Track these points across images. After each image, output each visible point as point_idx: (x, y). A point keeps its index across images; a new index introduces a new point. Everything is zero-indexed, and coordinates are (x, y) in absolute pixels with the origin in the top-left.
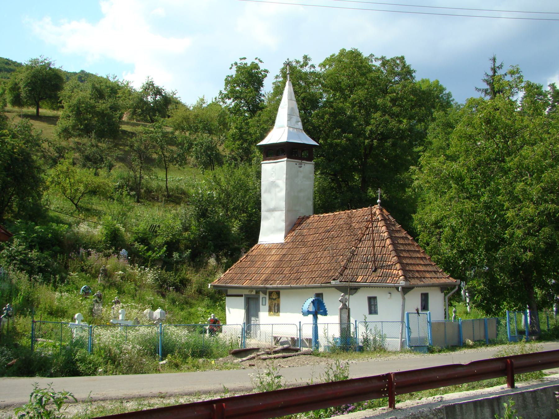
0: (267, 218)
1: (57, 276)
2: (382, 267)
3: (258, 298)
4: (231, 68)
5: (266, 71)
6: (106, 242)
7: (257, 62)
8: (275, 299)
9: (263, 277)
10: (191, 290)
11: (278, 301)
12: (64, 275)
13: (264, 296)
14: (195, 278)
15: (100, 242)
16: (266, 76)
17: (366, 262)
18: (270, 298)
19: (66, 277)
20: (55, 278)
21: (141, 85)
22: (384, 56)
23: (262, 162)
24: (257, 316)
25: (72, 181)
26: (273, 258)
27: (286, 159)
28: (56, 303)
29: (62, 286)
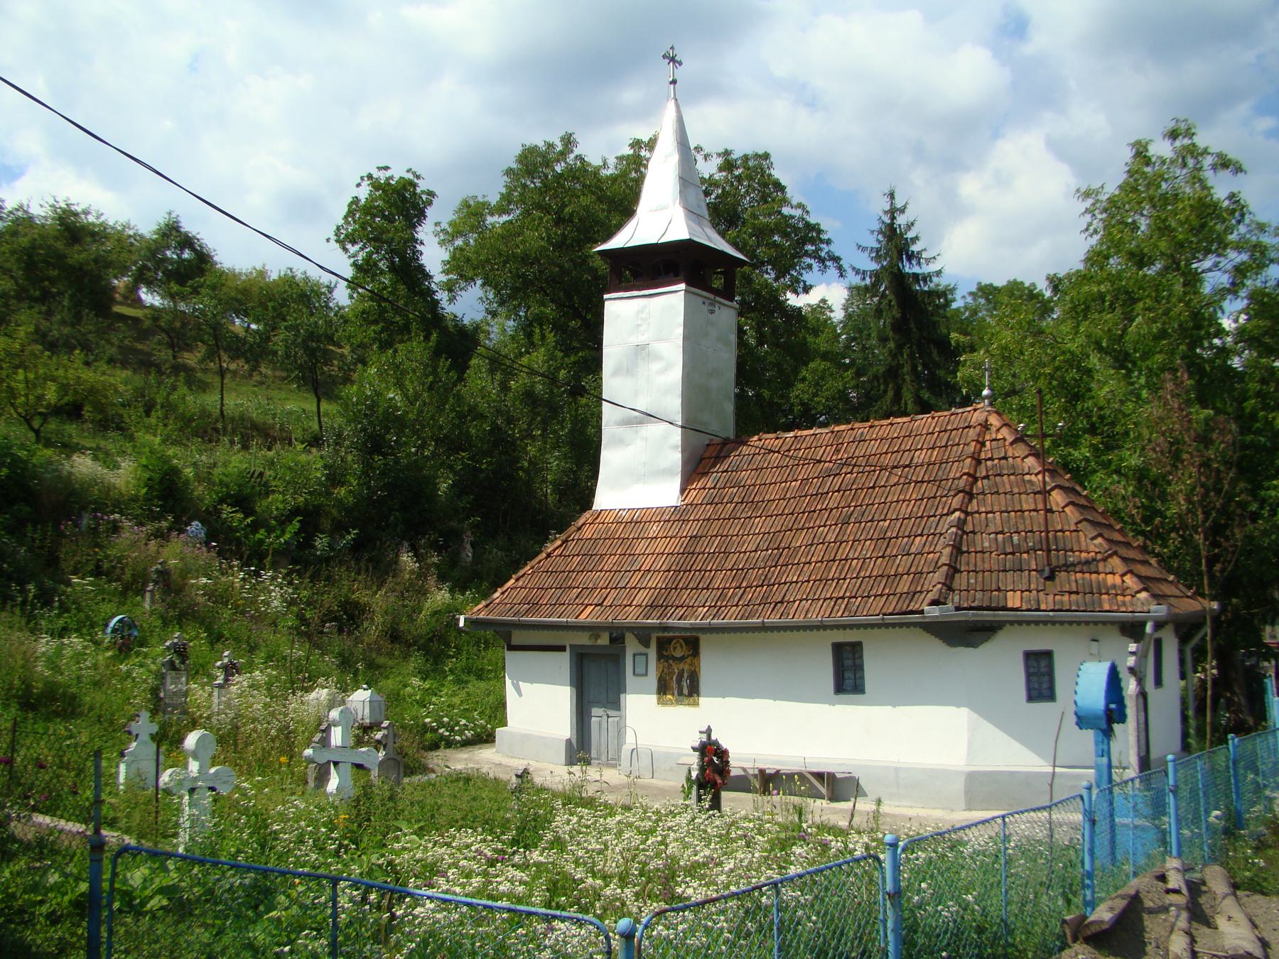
0: (621, 442)
1: (31, 587)
2: (1068, 567)
3: (618, 655)
4: (359, 185)
5: (431, 194)
6: (148, 499)
7: (410, 176)
8: (682, 659)
9: (642, 598)
10: (373, 629)
11: (691, 665)
12: (49, 583)
13: (642, 649)
14: (379, 601)
15: (135, 499)
16: (430, 203)
17: (1013, 553)
18: (660, 656)
19: (54, 591)
20: (23, 591)
21: (155, 227)
22: (729, 149)
23: (606, 296)
24: (614, 703)
25: (31, 376)
26: (660, 546)
27: (682, 286)
28: (41, 668)
29: (47, 618)
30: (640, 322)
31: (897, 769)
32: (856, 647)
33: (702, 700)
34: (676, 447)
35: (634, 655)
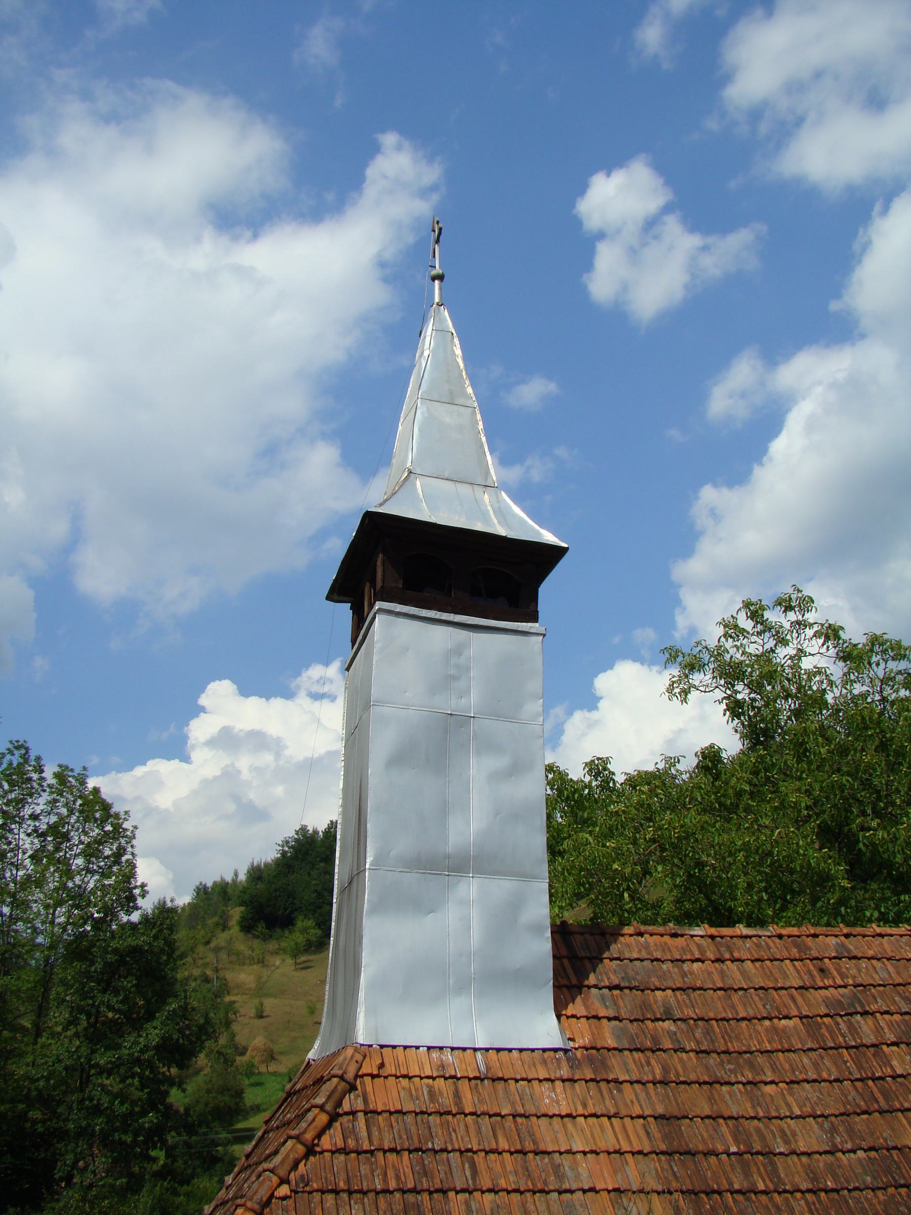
23: (378, 605)
30: (452, 671)
34: (536, 929)
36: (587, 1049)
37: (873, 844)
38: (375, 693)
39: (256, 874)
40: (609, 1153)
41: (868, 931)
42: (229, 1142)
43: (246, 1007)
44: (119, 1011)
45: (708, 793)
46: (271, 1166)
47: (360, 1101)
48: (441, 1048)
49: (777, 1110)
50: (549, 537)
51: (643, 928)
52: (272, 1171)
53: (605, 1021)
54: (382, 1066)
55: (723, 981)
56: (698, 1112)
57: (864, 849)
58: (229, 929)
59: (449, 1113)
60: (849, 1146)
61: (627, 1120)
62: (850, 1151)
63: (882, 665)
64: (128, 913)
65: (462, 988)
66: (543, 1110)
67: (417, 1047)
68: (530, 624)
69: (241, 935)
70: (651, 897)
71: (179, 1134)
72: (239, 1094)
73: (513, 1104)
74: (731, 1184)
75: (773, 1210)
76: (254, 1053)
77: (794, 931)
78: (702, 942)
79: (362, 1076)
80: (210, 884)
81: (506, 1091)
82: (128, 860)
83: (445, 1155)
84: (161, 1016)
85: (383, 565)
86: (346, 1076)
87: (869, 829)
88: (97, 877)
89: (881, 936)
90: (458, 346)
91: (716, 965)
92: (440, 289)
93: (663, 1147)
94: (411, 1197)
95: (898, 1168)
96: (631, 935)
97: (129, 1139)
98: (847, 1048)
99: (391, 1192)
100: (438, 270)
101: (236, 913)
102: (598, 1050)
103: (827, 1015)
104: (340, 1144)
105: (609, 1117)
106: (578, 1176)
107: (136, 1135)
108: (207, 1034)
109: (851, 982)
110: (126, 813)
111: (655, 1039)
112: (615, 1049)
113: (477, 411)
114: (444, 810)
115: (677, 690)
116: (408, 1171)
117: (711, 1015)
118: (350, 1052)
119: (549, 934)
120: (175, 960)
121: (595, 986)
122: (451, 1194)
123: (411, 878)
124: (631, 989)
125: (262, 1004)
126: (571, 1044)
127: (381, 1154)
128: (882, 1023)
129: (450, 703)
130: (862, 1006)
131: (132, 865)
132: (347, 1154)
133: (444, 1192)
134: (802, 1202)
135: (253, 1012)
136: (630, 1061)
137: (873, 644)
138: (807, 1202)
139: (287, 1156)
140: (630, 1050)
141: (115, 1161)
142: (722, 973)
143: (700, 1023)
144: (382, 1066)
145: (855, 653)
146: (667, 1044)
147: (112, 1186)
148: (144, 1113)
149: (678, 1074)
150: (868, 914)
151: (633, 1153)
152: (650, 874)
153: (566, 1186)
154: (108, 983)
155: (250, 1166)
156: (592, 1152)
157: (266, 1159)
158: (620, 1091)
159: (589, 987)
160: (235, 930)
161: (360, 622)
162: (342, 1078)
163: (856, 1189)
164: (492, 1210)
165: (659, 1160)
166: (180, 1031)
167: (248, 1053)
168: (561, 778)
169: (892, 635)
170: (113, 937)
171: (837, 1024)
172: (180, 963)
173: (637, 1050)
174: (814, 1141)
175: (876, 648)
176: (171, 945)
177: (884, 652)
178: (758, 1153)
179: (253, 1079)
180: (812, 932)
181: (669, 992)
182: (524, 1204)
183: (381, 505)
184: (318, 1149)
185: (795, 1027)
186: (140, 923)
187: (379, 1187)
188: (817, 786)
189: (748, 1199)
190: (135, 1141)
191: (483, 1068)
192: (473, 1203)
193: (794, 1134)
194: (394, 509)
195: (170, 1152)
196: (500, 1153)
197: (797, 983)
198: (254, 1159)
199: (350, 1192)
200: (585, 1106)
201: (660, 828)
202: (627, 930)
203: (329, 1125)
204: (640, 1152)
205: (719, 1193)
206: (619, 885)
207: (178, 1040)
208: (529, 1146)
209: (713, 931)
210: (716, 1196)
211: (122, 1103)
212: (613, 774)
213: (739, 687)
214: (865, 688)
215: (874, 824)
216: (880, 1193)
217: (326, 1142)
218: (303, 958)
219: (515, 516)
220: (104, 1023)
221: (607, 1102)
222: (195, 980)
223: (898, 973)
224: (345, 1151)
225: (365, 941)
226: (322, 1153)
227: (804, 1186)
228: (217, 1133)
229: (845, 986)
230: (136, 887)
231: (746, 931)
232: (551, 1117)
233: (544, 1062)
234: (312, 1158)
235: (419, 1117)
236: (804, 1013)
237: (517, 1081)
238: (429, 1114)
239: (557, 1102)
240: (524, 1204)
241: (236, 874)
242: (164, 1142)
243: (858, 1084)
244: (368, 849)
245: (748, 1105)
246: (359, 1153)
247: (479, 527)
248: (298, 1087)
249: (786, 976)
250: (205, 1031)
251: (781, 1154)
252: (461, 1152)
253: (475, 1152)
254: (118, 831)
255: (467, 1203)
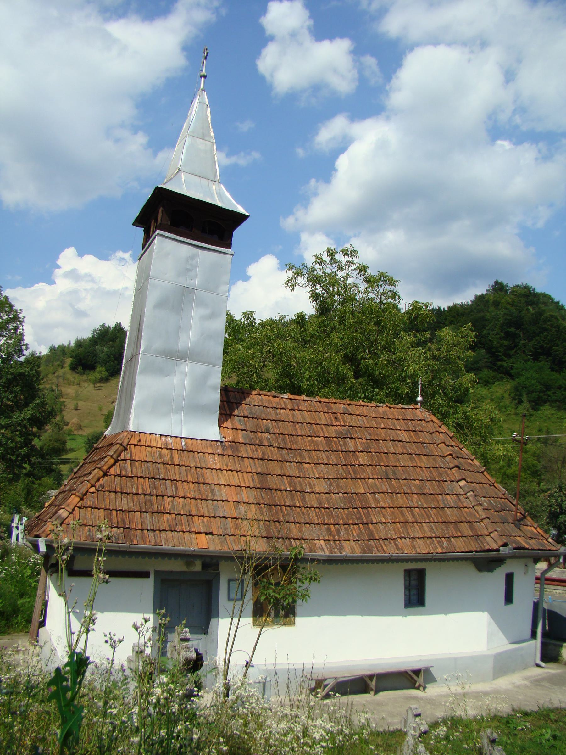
23: (158, 232)
30: (189, 267)
31: (456, 659)
32: (421, 574)
33: (298, 620)
34: (214, 388)
35: (229, 581)
36: (231, 442)
37: (367, 366)
38: (152, 273)
39: (79, 344)
40: (235, 486)
41: (358, 403)
42: (59, 464)
43: (70, 405)
44: (12, 401)
45: (297, 334)
46: (88, 479)
47: (129, 455)
48: (166, 436)
49: (309, 474)
50: (241, 210)
51: (261, 392)
52: (88, 481)
53: (240, 431)
54: (139, 441)
55: (293, 419)
56: (275, 473)
57: (362, 367)
58: (65, 368)
59: (167, 464)
60: (336, 491)
61: (245, 473)
62: (336, 493)
63: (383, 286)
64: (19, 357)
65: (178, 410)
66: (209, 466)
67: (156, 435)
68: (227, 249)
69: (70, 371)
70: (265, 376)
71: (37, 458)
72: (64, 443)
73: (196, 462)
74: (285, 503)
75: (301, 514)
76: (72, 425)
77: (327, 400)
78: (286, 401)
79: (130, 445)
80: (57, 346)
81: (193, 457)
82: (20, 332)
83: (164, 481)
84: (32, 405)
85: (162, 213)
86: (123, 444)
87: (366, 359)
88: (5, 338)
89: (363, 406)
90: (209, 112)
91: (291, 411)
92: (204, 82)
93: (259, 486)
94: (148, 497)
95: (355, 501)
96: (255, 395)
97: (14, 458)
98: (341, 452)
99: (140, 495)
100: (204, 73)
101: (68, 361)
102: (235, 443)
103: (335, 437)
104: (119, 473)
105: (237, 472)
106: (221, 495)
107: (18, 457)
108: (52, 415)
109: (347, 424)
110: (21, 310)
111: (261, 441)
112: (243, 443)
113: (215, 145)
114: (178, 331)
115: (290, 284)
116: (148, 486)
117: (286, 433)
118: (126, 433)
119: (219, 391)
120: (40, 380)
121: (237, 416)
122: (166, 498)
123: (160, 359)
124: (253, 418)
125: (77, 404)
126: (224, 439)
127: (136, 478)
128: (358, 443)
129: (186, 282)
130: (351, 435)
131: (22, 335)
132: (121, 477)
133: (163, 496)
134: (314, 512)
135: (73, 407)
136: (249, 448)
137: (381, 277)
138: (316, 512)
139: (95, 475)
140: (250, 444)
141: (7, 467)
142: (293, 415)
143: (281, 435)
144: (139, 441)
145: (372, 279)
146: (266, 443)
147: (6, 478)
148: (22, 448)
149: (269, 456)
150: (359, 395)
151: (246, 487)
152: (266, 367)
153: (216, 498)
154: (8, 388)
155: (76, 477)
156: (228, 485)
157: (85, 475)
158: (243, 461)
159: (234, 416)
160: (67, 368)
161: (148, 237)
162: (121, 444)
163: (336, 508)
164: (183, 505)
165: (256, 491)
166: (40, 413)
167: (70, 425)
168: (231, 318)
169: (390, 274)
170: (11, 367)
171: (339, 441)
172: (42, 382)
173: (252, 444)
174: (322, 488)
175: (382, 279)
176: (38, 373)
177: (385, 281)
178: (298, 491)
179: (71, 437)
180: (334, 401)
181: (269, 421)
182: (197, 504)
183: (164, 184)
184: (109, 474)
185: (321, 441)
186: (24, 362)
187: (134, 492)
188: (346, 337)
189: (292, 509)
190: (16, 459)
191: (184, 446)
192: (175, 502)
193: (314, 485)
194: (169, 187)
195: (32, 465)
196: (188, 482)
197: (324, 422)
198: (77, 475)
199: (122, 493)
200: (227, 466)
201: (274, 347)
202: (254, 392)
203: (114, 464)
204: (249, 487)
205: (280, 506)
206: (251, 371)
207: (39, 417)
208: (201, 480)
209: (292, 397)
210: (278, 507)
211: (12, 442)
212: (255, 319)
213: (318, 287)
214: (374, 296)
215: (368, 357)
216: (346, 510)
217: (112, 471)
218: (98, 385)
219: (226, 197)
220: (5, 406)
221: (237, 465)
222: (47, 389)
223: (368, 422)
224: (120, 476)
225: (137, 385)
226: (110, 475)
227: (315, 506)
228: (53, 459)
229: (345, 426)
230: (23, 345)
231: (306, 398)
232: (212, 469)
233: (211, 446)
234: (106, 477)
235: (154, 464)
236: (326, 435)
237: (198, 453)
238: (159, 464)
239: (215, 463)
240: (197, 504)
241: (70, 343)
242: (30, 461)
243: (344, 467)
244: (142, 345)
245: (297, 472)
246: (127, 477)
247: (208, 200)
248: (100, 446)
249: (320, 419)
250: (52, 414)
251: (308, 492)
252: (172, 481)
253: (177, 481)
254: (16, 318)
255: (172, 502)
